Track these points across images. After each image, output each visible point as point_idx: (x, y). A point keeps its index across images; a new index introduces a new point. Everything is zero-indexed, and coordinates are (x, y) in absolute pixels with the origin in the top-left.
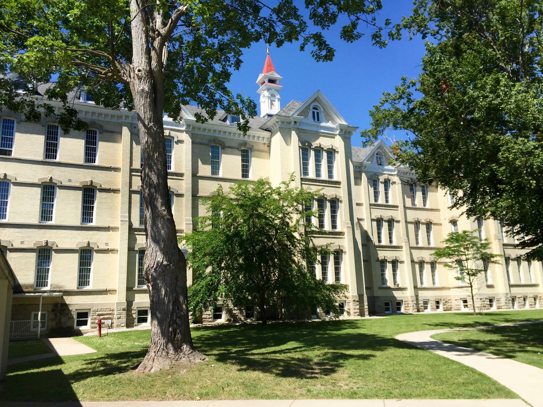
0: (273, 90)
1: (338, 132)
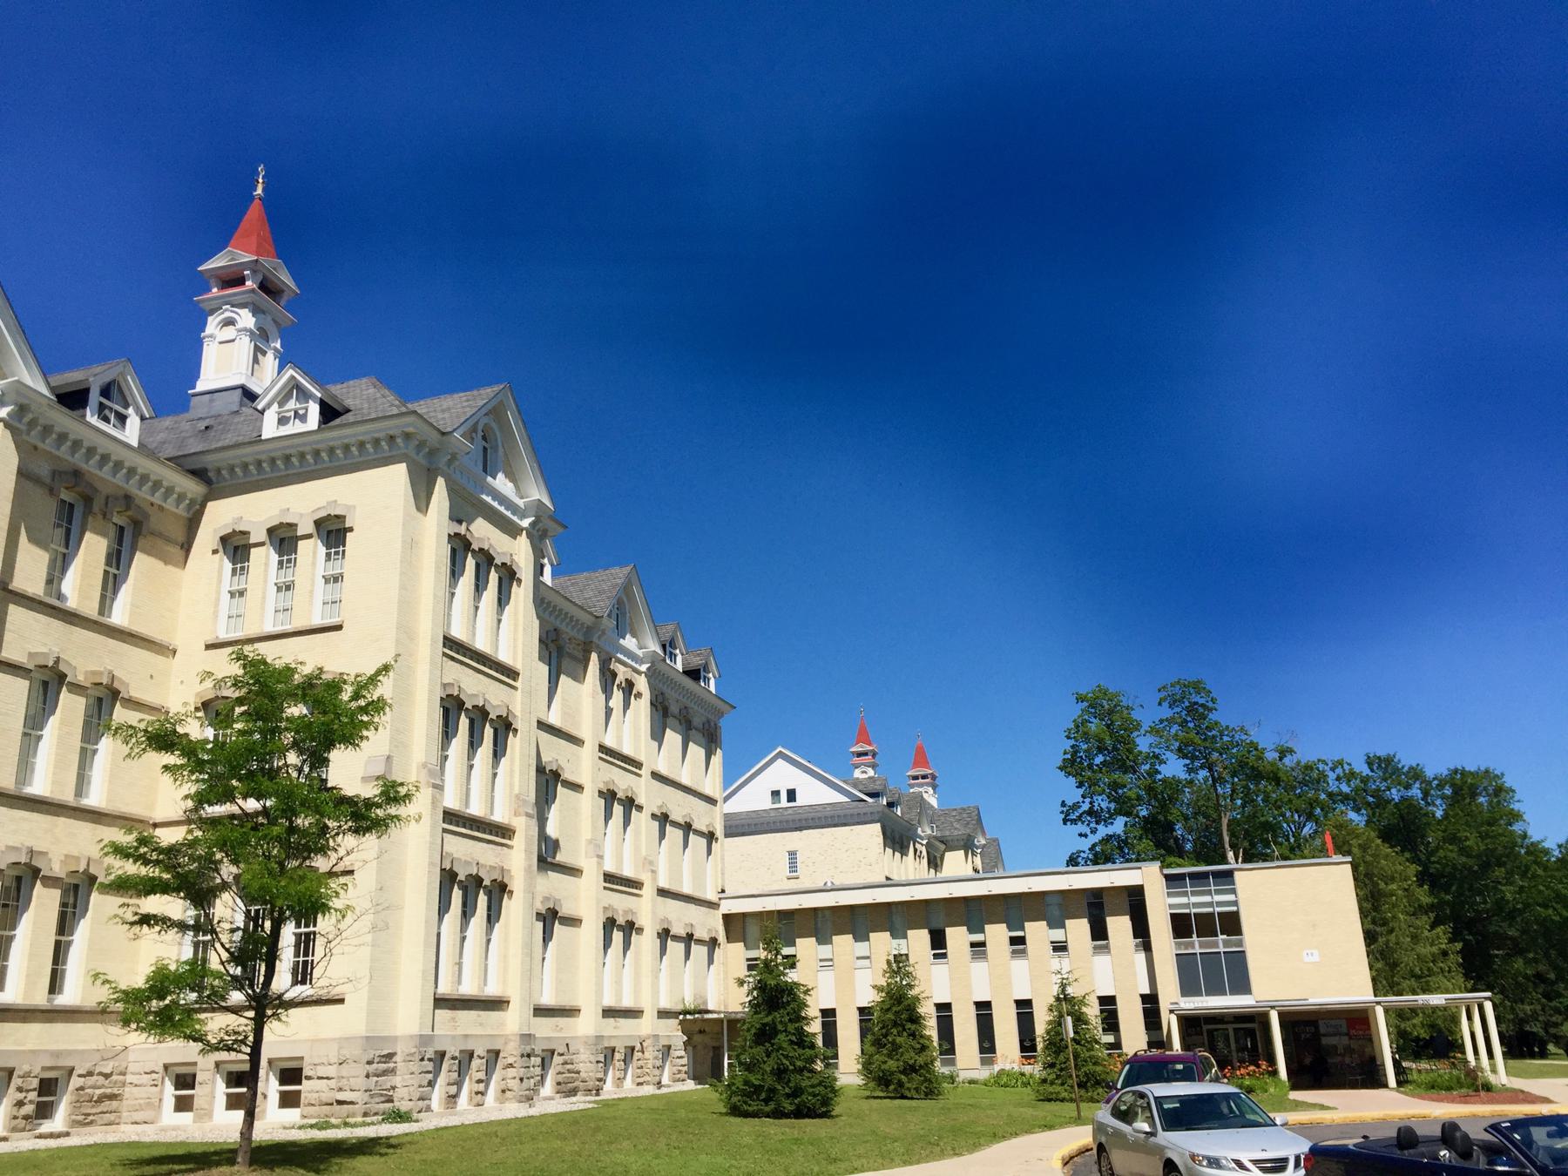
0: (269, 318)
1: (525, 523)
